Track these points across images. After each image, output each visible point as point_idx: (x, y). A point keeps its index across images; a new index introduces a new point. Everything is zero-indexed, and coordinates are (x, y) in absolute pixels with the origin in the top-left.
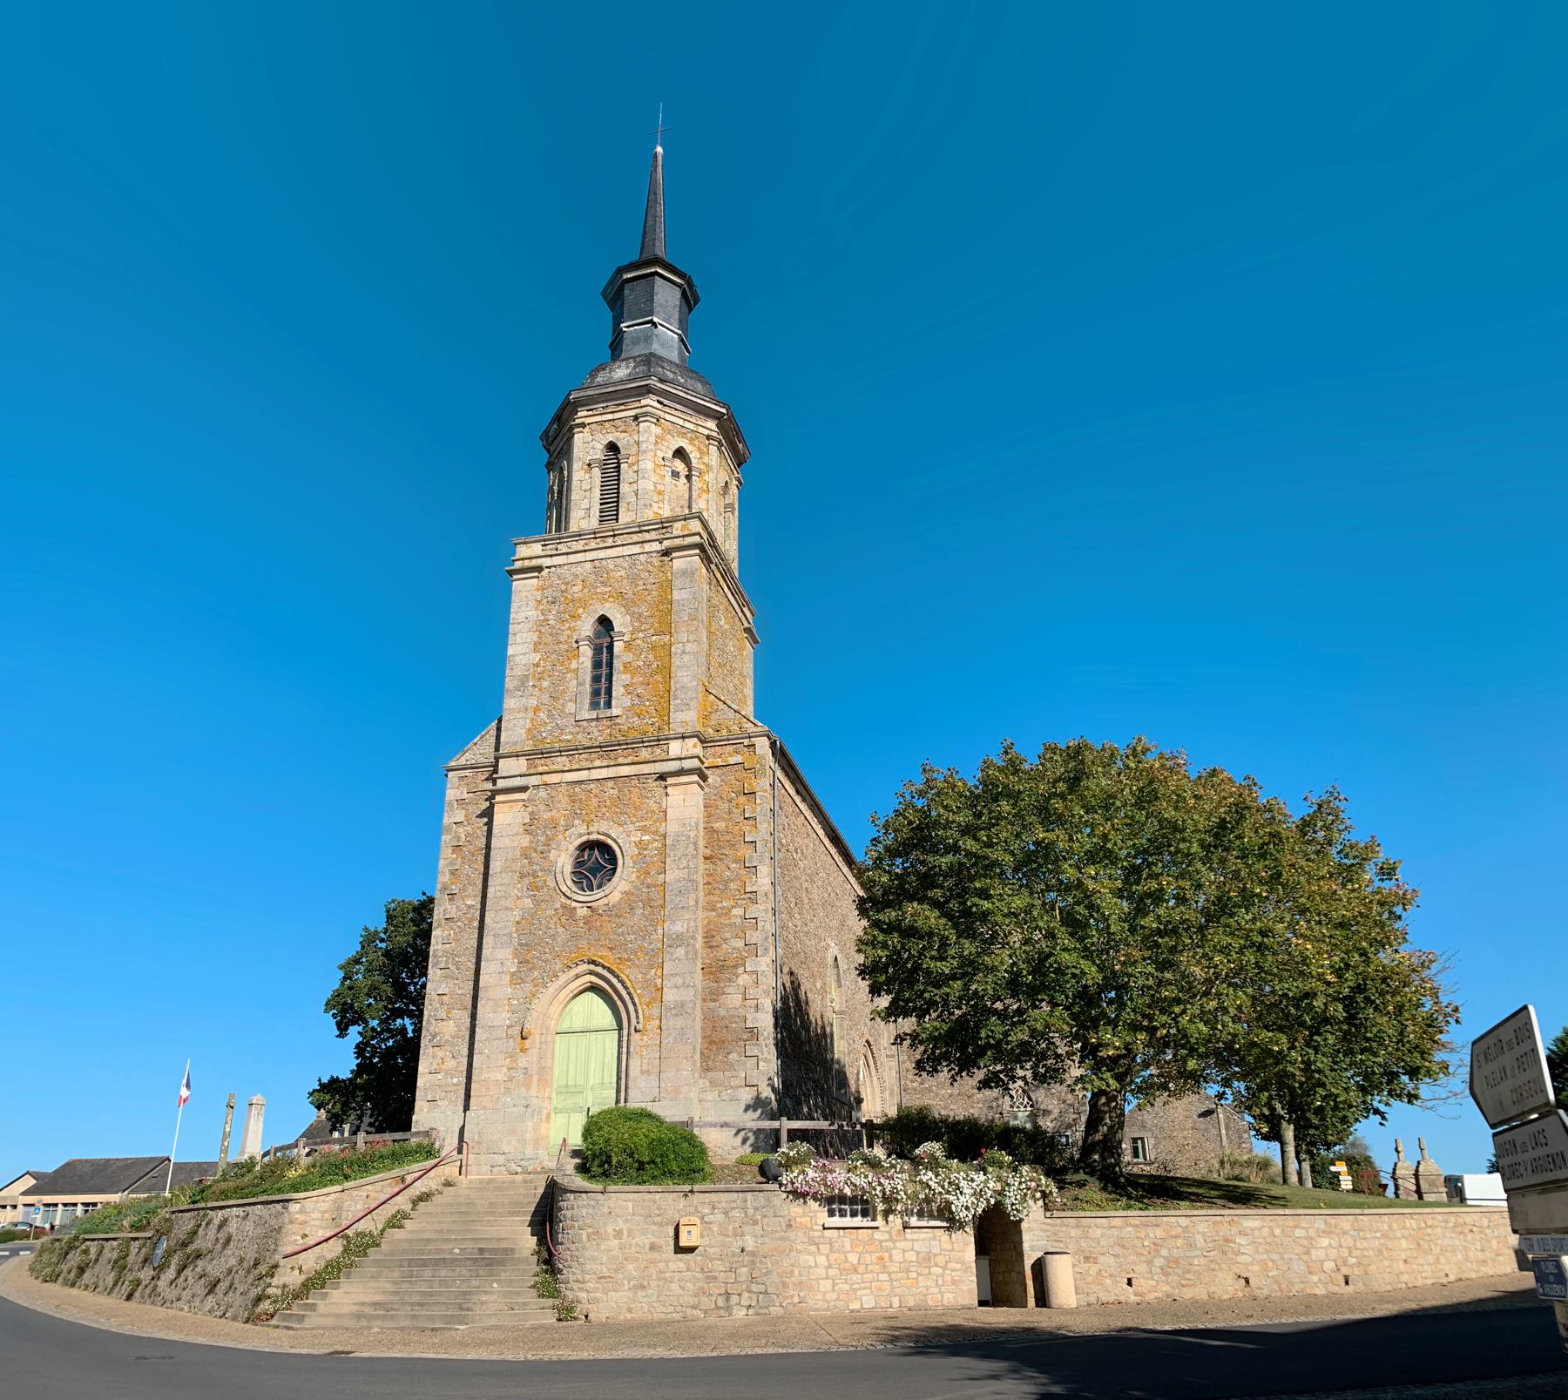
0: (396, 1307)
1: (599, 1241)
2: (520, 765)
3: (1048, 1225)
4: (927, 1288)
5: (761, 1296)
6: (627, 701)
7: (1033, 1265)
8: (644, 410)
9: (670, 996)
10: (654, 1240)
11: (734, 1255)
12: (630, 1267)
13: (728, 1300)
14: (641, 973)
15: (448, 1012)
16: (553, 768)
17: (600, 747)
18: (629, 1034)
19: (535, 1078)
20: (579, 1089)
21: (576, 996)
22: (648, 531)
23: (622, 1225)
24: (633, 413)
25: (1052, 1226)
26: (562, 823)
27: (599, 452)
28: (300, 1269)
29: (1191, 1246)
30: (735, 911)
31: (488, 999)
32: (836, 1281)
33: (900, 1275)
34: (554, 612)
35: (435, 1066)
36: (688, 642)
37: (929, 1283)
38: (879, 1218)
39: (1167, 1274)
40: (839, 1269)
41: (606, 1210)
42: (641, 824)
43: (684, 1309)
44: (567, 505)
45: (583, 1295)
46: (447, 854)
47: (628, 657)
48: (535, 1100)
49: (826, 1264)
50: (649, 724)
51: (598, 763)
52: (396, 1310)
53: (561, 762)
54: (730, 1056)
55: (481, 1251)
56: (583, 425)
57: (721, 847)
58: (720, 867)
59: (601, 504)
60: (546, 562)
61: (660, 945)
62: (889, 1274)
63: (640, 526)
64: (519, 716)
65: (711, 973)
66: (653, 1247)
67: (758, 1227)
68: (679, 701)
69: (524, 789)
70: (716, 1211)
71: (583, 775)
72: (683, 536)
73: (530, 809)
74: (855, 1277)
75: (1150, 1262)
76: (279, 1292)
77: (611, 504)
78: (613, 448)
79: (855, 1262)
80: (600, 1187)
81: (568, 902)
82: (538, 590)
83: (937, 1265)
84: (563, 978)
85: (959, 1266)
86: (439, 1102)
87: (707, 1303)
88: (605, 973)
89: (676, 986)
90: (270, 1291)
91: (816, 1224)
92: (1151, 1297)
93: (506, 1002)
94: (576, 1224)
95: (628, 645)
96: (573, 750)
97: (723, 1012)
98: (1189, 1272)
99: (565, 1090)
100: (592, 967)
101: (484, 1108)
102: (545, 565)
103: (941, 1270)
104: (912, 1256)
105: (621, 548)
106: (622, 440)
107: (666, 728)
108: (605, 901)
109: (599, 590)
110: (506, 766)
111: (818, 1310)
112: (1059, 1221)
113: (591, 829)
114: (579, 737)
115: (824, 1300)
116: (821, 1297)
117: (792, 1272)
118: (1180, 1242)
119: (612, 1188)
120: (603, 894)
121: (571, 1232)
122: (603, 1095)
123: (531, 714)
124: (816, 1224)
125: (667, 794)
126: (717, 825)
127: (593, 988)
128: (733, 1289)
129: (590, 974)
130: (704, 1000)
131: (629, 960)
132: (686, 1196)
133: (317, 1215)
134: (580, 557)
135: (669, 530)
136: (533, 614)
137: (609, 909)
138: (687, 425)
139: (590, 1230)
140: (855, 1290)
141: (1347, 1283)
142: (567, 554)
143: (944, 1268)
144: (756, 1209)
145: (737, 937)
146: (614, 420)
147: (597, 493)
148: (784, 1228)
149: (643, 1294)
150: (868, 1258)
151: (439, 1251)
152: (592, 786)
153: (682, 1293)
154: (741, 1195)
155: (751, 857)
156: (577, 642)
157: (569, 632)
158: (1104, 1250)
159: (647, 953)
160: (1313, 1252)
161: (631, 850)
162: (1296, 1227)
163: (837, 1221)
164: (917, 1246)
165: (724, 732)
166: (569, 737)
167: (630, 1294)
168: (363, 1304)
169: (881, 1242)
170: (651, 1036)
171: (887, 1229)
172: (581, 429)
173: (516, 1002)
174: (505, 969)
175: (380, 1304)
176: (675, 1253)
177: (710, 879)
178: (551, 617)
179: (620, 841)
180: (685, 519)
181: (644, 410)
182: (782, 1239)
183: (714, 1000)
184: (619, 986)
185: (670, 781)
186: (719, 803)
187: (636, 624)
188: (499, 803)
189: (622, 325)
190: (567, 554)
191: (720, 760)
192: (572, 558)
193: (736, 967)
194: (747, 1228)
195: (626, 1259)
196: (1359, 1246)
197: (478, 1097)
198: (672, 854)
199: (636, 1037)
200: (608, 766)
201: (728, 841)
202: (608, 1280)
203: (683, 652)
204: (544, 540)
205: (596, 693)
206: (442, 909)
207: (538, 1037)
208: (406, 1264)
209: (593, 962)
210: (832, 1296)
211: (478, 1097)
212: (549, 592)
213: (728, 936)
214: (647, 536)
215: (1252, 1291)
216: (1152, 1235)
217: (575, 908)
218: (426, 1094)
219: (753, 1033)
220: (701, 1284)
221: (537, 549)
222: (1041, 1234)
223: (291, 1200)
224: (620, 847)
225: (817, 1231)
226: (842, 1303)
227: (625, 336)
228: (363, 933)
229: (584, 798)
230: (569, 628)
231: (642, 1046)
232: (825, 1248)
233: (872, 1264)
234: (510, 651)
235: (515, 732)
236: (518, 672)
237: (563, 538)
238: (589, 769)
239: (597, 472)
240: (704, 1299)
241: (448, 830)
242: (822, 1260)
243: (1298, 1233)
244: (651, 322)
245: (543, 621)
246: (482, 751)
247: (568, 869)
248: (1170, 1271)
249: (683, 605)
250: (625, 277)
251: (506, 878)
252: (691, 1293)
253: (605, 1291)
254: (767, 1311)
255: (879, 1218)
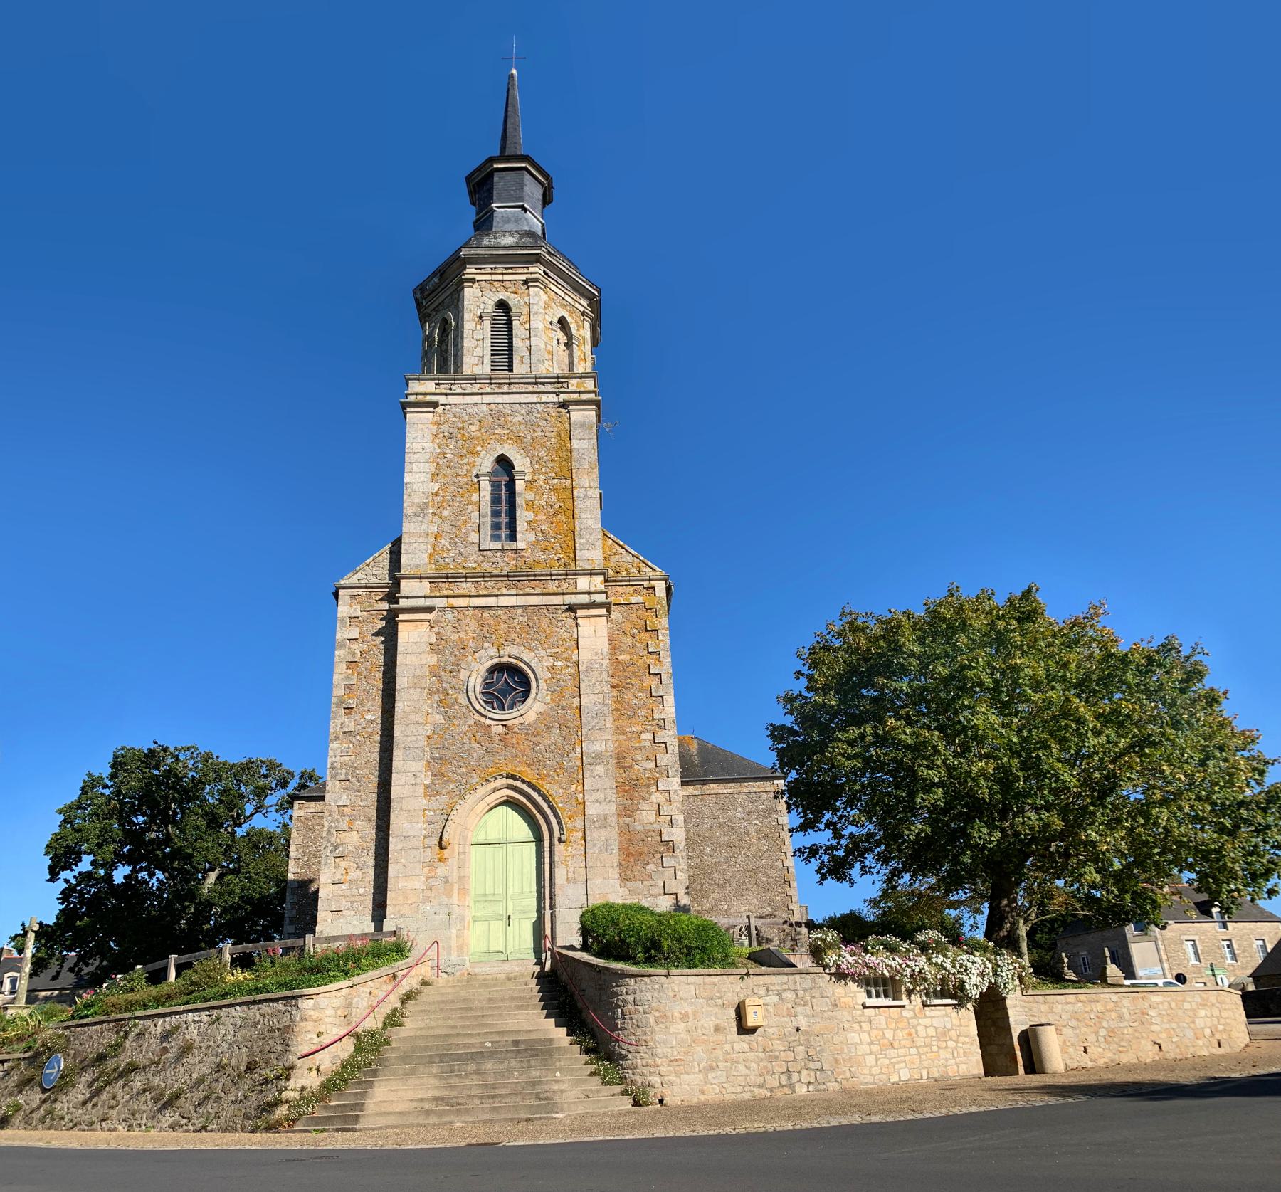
0: (461, 1101)
1: (667, 1025)
2: (424, 587)
3: (1025, 1001)
4: (947, 1060)
5: (818, 1073)
6: (531, 537)
7: (1019, 1037)
8: (534, 276)
9: (592, 810)
10: (718, 1022)
11: (790, 1034)
12: (699, 1049)
13: (789, 1078)
14: (561, 788)
15: (351, 823)
16: (457, 592)
17: (508, 576)
18: (551, 845)
19: (456, 887)
20: (498, 898)
21: (491, 809)
22: (543, 384)
23: (687, 1008)
24: (524, 277)
25: (1028, 1003)
26: (471, 644)
27: (490, 308)
28: (318, 1070)
29: (1121, 1018)
30: (644, 736)
31: (402, 810)
32: (879, 1056)
33: (925, 1049)
34: (451, 447)
35: (339, 876)
36: (590, 487)
37: (947, 1056)
38: (904, 997)
39: (1108, 1043)
40: (879, 1044)
41: (671, 994)
42: (553, 651)
43: (752, 1089)
44: (456, 356)
45: (655, 1080)
46: (340, 668)
47: (531, 496)
48: (456, 908)
49: (869, 1041)
50: (556, 558)
51: (505, 591)
52: (463, 1104)
53: (467, 587)
54: (648, 867)
55: (516, 1043)
56: (473, 281)
57: (627, 678)
58: (627, 696)
59: (492, 355)
60: (442, 399)
61: (579, 763)
62: (917, 1047)
63: (536, 378)
64: (420, 540)
65: (626, 791)
66: (717, 1029)
67: (809, 1008)
68: (583, 541)
69: (429, 610)
70: (770, 993)
71: (491, 601)
72: (580, 392)
73: (436, 629)
74: (893, 1052)
75: (1096, 1033)
76: (297, 1095)
77: (505, 354)
78: (503, 306)
79: (891, 1039)
80: (664, 972)
81: (483, 719)
82: (433, 424)
83: (951, 1039)
84: (481, 791)
85: (966, 1040)
86: (344, 913)
87: (772, 1082)
88: (524, 787)
89: (597, 801)
90: (285, 1095)
91: (857, 1004)
92: (1101, 1062)
93: (421, 813)
94: (641, 1008)
95: (529, 485)
96: (479, 577)
97: (639, 827)
98: (1122, 1040)
99: (483, 899)
100: (511, 782)
101: (402, 916)
102: (440, 402)
103: (954, 1044)
104: (932, 1032)
105: (518, 396)
106: (513, 300)
107: (573, 564)
108: (521, 720)
109: (496, 432)
110: (406, 587)
111: (867, 1083)
112: (1031, 998)
113: (501, 652)
114: (485, 565)
115: (871, 1075)
116: (868, 1072)
117: (842, 1048)
118: (1114, 1015)
119: (674, 971)
120: (518, 714)
121: (635, 1016)
122: (523, 904)
123: (432, 540)
124: (857, 1004)
125: (577, 625)
126: (621, 658)
127: (509, 802)
128: (793, 1067)
129: (507, 788)
130: (619, 815)
131: (549, 775)
132: (742, 979)
133: (330, 1012)
134: (476, 399)
135: (565, 385)
136: (429, 446)
137: (525, 728)
138: (567, 298)
139: (657, 1014)
140: (893, 1064)
141: (1220, 1046)
142: (463, 394)
143: (957, 1042)
144: (805, 990)
145: (647, 758)
146: (503, 281)
147: (488, 342)
148: (831, 1007)
149: (714, 1075)
150: (900, 1034)
151: (466, 1045)
152: (500, 612)
153: (748, 1072)
154: (790, 977)
155: (657, 688)
156: (477, 476)
157: (468, 467)
158: (1065, 1024)
159: (566, 770)
160: (1197, 1021)
161: (544, 674)
162: (1184, 1001)
163: (874, 1001)
164: (936, 1022)
165: (624, 574)
166: (474, 565)
167: (701, 1076)
168: (422, 1100)
169: (908, 1019)
170: (575, 846)
171: (911, 1007)
172: (471, 284)
173: (432, 813)
174: (419, 781)
175: (442, 1099)
176: (739, 1034)
177: (619, 706)
178: (448, 451)
179: (533, 665)
180: (581, 378)
181: (534, 276)
182: (829, 1018)
183: (629, 816)
184: (539, 800)
185: (580, 612)
186: (623, 637)
187: (537, 467)
188: (403, 621)
189: (493, 205)
190: (463, 394)
191: (621, 599)
192: (468, 399)
193: (648, 786)
194: (799, 1009)
195: (694, 1042)
196: (1223, 1015)
197: (395, 905)
198: (586, 679)
199: (559, 848)
200: (516, 595)
201: (633, 672)
202: (680, 1063)
203: (586, 496)
204: (439, 379)
205: (496, 527)
206: (339, 722)
207: (456, 846)
208: (437, 1060)
209: (513, 777)
210: (876, 1070)
211: (395, 905)
212: (445, 428)
213: (639, 757)
214: (542, 388)
215: (1164, 1055)
216: (1095, 1009)
217: (489, 726)
218: (330, 905)
219: (671, 847)
220: (765, 1064)
221: (430, 386)
222: (1021, 1010)
223: (301, 996)
224: (533, 671)
225: (858, 1010)
226: (884, 1077)
227: (495, 214)
228: (86, 779)
229: (493, 623)
230: (468, 463)
231: (566, 856)
232: (866, 1026)
233: (904, 1039)
234: (407, 478)
235: (415, 556)
236: (417, 498)
237: (458, 379)
238: (497, 596)
239: (487, 324)
240: (768, 1077)
241: (342, 646)
242: (865, 1037)
243: (1187, 1006)
244: (523, 207)
245: (439, 454)
246: (375, 573)
247: (479, 689)
248: (1110, 1039)
249: (583, 454)
250: (495, 166)
251: (415, 694)
252: (756, 1073)
253: (678, 1075)
254: (824, 1086)
255: (904, 997)
